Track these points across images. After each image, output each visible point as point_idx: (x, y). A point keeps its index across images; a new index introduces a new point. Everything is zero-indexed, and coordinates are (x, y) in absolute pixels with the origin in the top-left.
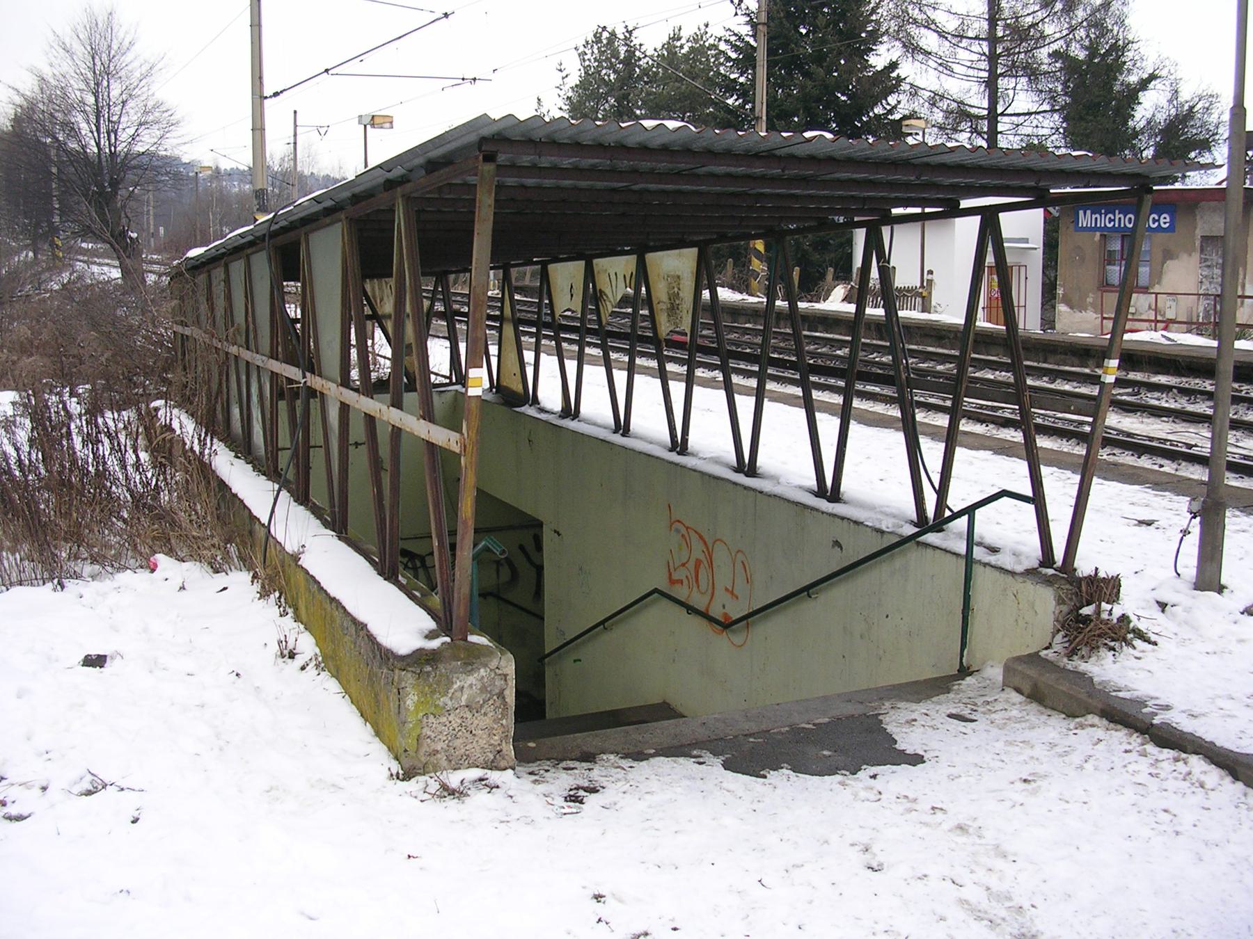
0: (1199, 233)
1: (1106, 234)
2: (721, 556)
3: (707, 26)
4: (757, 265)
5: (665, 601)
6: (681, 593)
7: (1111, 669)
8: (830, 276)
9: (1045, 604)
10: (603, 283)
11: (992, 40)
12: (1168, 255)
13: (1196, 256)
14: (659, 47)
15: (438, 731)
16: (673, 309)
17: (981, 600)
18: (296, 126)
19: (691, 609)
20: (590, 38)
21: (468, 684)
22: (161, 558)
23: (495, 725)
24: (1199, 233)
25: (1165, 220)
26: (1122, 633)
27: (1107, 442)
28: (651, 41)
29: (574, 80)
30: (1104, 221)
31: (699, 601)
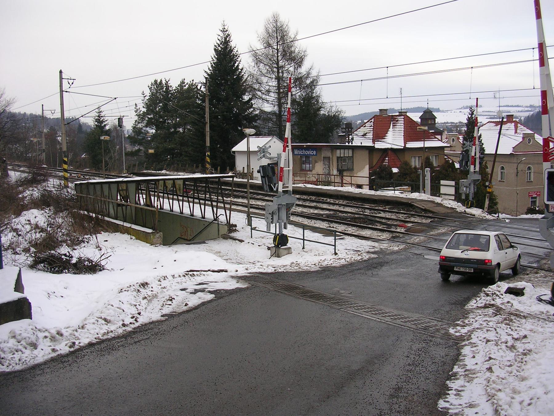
0: (322, 156)
1: (301, 156)
2: (189, 229)
3: (193, 81)
4: (208, 166)
5: (181, 240)
6: (183, 237)
7: (232, 235)
8: (228, 169)
9: (226, 228)
10: (167, 185)
11: (279, 93)
12: (316, 162)
13: (322, 162)
14: (177, 86)
15: (155, 240)
16: (180, 190)
17: (220, 229)
18: (43, 110)
19: (184, 239)
20: (153, 82)
21: (158, 235)
22: (102, 232)
23: (160, 240)
24: (322, 156)
25: (314, 152)
26: (235, 231)
27: (251, 208)
28: (174, 84)
29: (147, 98)
30: (300, 153)
31: (186, 238)
